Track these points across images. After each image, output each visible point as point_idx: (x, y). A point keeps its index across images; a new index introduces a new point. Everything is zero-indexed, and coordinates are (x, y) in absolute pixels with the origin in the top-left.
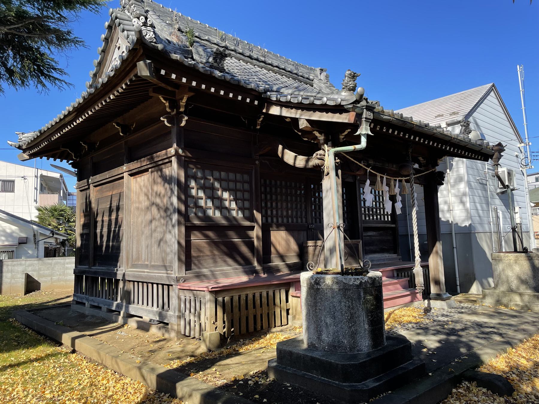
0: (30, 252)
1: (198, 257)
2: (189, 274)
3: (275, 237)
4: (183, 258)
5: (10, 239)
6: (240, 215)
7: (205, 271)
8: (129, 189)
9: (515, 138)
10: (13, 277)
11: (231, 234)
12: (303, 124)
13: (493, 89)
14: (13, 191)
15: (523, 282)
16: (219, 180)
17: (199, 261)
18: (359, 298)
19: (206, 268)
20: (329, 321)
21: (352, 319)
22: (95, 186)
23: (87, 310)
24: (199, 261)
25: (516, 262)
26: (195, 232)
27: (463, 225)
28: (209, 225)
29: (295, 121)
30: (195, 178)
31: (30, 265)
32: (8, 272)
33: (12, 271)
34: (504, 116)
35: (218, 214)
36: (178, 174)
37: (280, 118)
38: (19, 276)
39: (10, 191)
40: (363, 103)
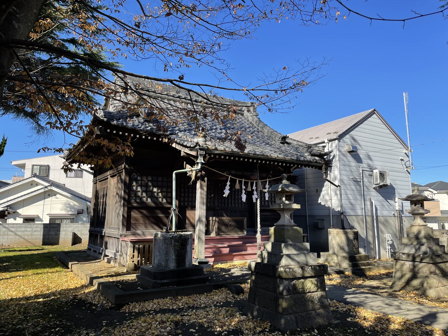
0: (84, 219)
1: (135, 224)
2: (128, 233)
3: (190, 215)
4: (125, 224)
5: (73, 210)
6: (165, 201)
7: (139, 232)
8: (110, 184)
9: (402, 146)
10: (66, 235)
11: (158, 211)
12: (182, 154)
13: (375, 113)
14: (82, 177)
15: (342, 248)
16: (151, 181)
17: (136, 226)
18: (171, 244)
19: (140, 230)
20: (158, 254)
21: (167, 254)
22: (100, 182)
23: (92, 253)
24: (136, 226)
25: (337, 234)
26: (134, 210)
27: (337, 210)
28: (143, 206)
29: (180, 151)
30: (136, 181)
31: (76, 227)
32: (63, 231)
33: (65, 231)
34: (388, 131)
35: (149, 200)
36: (125, 179)
37: (175, 149)
38: (69, 234)
39: (80, 177)
40: (198, 147)
